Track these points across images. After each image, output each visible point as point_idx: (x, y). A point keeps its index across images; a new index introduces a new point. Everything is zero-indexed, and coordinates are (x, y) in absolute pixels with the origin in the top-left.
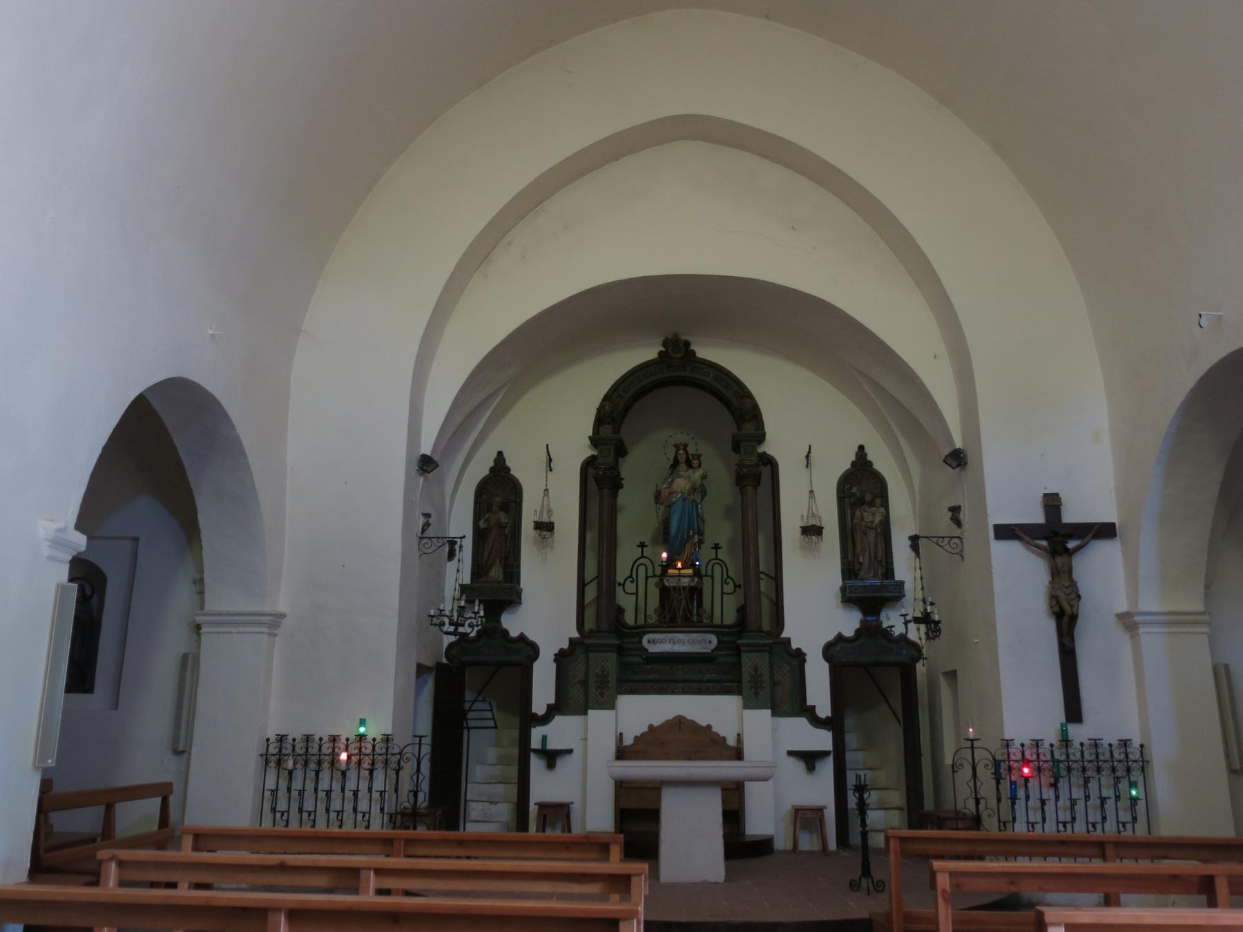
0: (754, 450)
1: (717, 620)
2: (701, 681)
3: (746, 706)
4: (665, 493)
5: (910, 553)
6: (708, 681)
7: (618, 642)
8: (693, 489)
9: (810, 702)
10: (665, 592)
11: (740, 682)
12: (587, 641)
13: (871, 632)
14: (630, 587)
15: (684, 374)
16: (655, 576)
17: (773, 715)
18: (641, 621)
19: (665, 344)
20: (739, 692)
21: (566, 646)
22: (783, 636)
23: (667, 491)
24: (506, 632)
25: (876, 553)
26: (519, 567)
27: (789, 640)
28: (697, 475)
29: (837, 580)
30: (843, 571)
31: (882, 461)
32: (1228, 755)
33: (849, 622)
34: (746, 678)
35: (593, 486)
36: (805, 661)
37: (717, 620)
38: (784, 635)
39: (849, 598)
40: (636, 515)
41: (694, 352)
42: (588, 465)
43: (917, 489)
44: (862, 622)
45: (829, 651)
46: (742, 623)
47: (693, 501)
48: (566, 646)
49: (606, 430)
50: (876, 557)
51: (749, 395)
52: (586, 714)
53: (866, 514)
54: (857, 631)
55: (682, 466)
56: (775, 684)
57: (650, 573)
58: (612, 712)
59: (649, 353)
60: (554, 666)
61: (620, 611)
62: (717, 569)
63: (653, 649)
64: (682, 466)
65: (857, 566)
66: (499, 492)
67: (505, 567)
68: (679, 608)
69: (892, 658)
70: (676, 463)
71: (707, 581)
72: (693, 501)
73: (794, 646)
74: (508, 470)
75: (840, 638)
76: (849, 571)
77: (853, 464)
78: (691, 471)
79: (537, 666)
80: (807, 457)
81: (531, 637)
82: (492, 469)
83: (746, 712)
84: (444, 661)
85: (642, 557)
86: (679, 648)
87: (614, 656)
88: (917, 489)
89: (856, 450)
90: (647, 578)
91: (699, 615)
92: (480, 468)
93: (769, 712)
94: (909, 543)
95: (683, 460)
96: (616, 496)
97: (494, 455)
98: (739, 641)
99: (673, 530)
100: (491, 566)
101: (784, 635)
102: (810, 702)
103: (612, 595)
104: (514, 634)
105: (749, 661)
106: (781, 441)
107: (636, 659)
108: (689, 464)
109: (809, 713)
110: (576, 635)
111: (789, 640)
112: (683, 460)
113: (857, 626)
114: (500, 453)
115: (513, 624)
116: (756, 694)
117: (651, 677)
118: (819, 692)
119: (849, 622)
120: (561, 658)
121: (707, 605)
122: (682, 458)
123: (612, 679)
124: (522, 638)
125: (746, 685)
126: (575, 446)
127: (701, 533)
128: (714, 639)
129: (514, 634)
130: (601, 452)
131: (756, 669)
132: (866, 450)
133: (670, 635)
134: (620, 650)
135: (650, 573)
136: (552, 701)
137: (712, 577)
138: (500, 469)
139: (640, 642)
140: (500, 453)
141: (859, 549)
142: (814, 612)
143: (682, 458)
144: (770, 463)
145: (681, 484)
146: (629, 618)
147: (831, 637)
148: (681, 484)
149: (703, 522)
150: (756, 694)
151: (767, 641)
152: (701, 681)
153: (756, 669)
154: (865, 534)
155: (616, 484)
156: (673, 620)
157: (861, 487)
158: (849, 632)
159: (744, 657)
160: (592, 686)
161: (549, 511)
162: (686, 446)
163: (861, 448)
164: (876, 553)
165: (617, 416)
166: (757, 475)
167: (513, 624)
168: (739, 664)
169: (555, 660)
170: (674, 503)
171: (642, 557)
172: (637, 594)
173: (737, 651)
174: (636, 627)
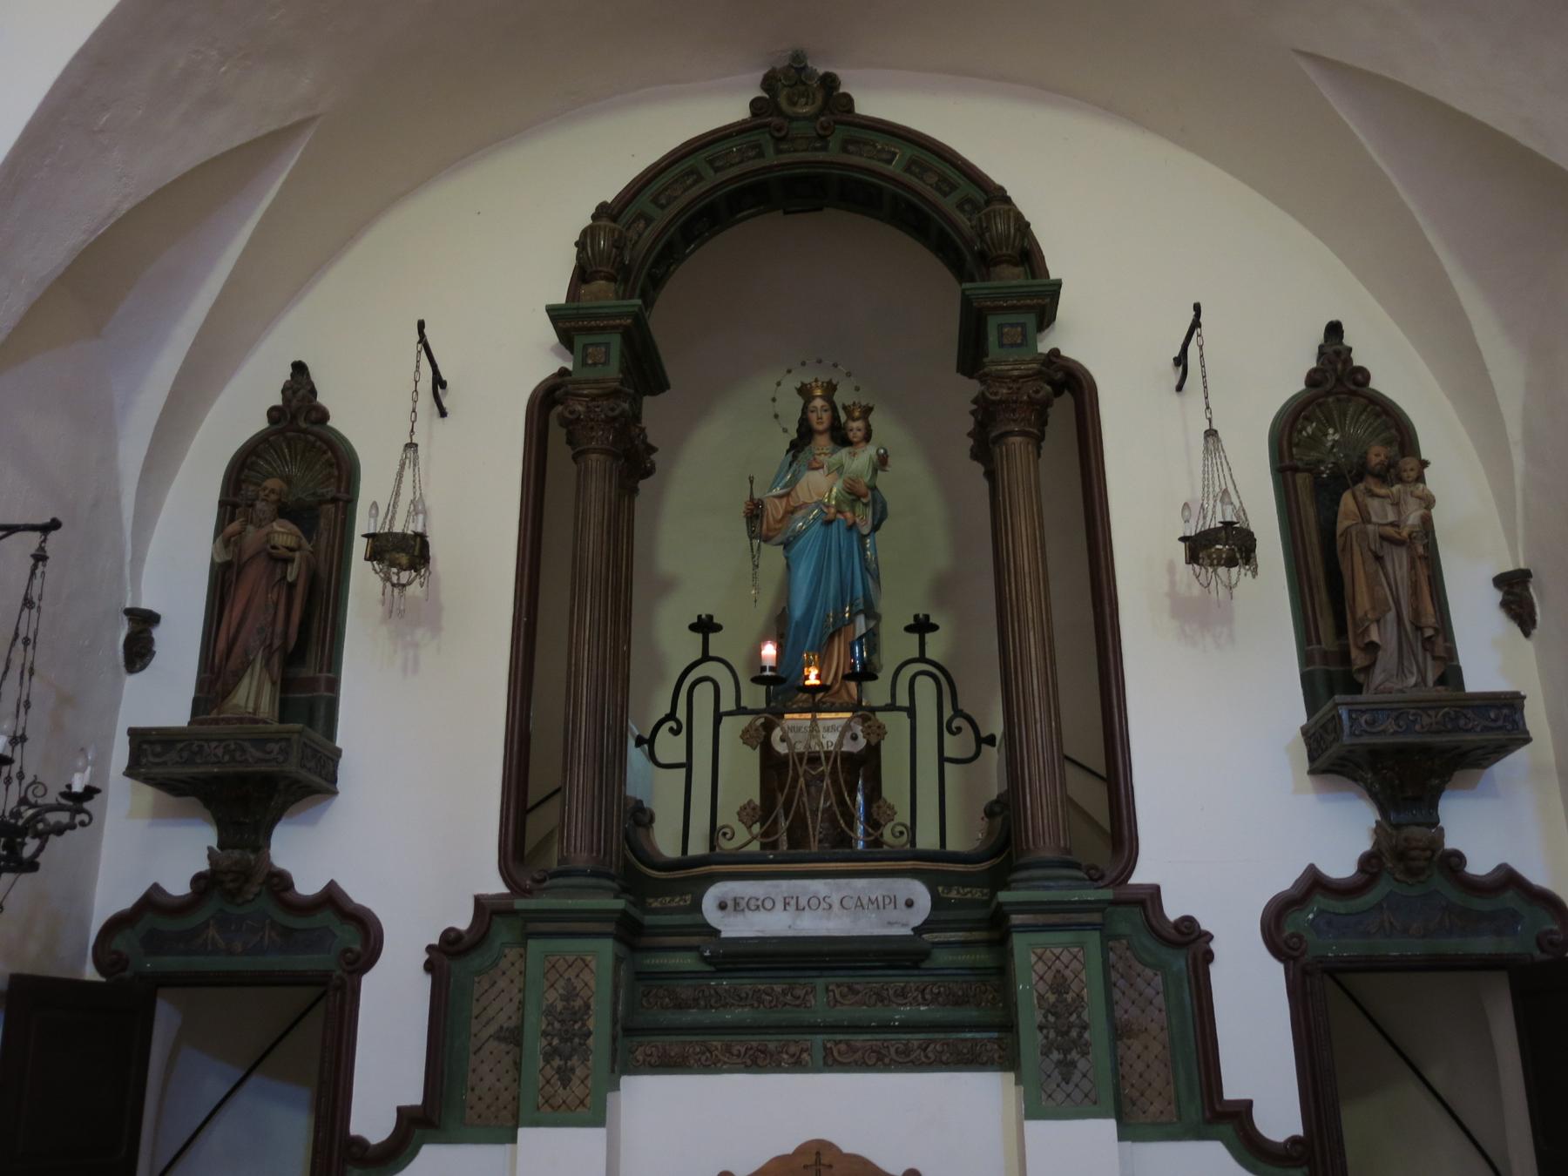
0: (1026, 341)
1: (927, 839)
2: (885, 1027)
3: (1033, 1111)
4: (774, 510)
5: (1500, 624)
6: (908, 1027)
7: (619, 904)
8: (853, 495)
9: (1232, 1091)
10: (773, 767)
11: (1008, 1027)
12: (520, 904)
13: (1409, 857)
14: (670, 747)
15: (821, 156)
16: (740, 710)
17: (1122, 1136)
18: (698, 847)
19: (769, 83)
20: (1006, 1059)
21: (463, 920)
22: (1137, 878)
23: (781, 506)
24: (281, 882)
25: (1417, 613)
26: (334, 685)
27: (1155, 891)
28: (859, 461)
29: (1289, 710)
30: (1307, 681)
31: (1395, 369)
32: (615, 1004)
33: (1337, 834)
34: (1029, 1017)
35: (557, 435)
36: (1209, 956)
37: (927, 839)
38: (1141, 876)
39: (1331, 756)
40: (701, 562)
41: (848, 100)
42: (546, 403)
43: (1514, 430)
44: (1379, 830)
45: (1282, 925)
46: (1006, 841)
47: (852, 527)
48: (463, 921)
49: (602, 293)
50: (1418, 628)
51: (999, 196)
52: (513, 1139)
53: (1374, 505)
54: (1366, 862)
55: (822, 442)
56: (1119, 1032)
57: (727, 704)
58: (599, 1134)
59: (731, 109)
60: (427, 980)
61: (641, 817)
62: (925, 687)
63: (734, 927)
64: (822, 442)
65: (1358, 658)
66: (295, 479)
67: (286, 684)
68: (817, 812)
69: (1484, 945)
70: (805, 434)
71: (895, 723)
72: (852, 527)
73: (1173, 910)
74: (324, 416)
75: (1314, 883)
76: (1330, 672)
77: (1313, 379)
78: (843, 453)
79: (370, 984)
80: (1181, 360)
81: (359, 895)
82: (274, 414)
83: (1037, 1130)
84: (90, 973)
85: (706, 657)
86: (812, 925)
87: (606, 949)
88: (1514, 430)
89: (1319, 337)
90: (718, 717)
91: (873, 824)
92: (241, 411)
93: (1110, 1125)
94: (1497, 596)
95: (822, 429)
96: (633, 491)
97: (286, 374)
98: (1003, 896)
99: (798, 611)
100: (238, 677)
101: (1141, 876)
102: (1232, 1091)
103: (612, 766)
104: (307, 885)
105: (1034, 958)
106: (1103, 322)
107: (686, 961)
108: (841, 438)
109: (1233, 1123)
110: (495, 886)
111: (1155, 891)
112: (822, 429)
113: (1366, 845)
114: (299, 368)
115: (306, 854)
116: (1067, 1067)
117: (728, 1016)
118: (1258, 1053)
119: (1337, 834)
120: (447, 956)
121: (894, 787)
122: (820, 420)
123: (599, 1024)
124: (332, 898)
125: (1030, 1040)
126: (511, 350)
127: (871, 612)
128: (920, 893)
129: (307, 885)
130: (583, 363)
131: (1059, 985)
132: (1348, 340)
133: (785, 886)
134: (629, 932)
135: (727, 704)
136: (414, 1097)
137: (911, 711)
138: (299, 422)
139: (697, 906)
140: (299, 368)
141: (1363, 603)
142: (1226, 798)
143: (820, 420)
144: (1073, 384)
145: (816, 488)
146: (666, 841)
147: (1284, 880)
148: (816, 488)
149: (877, 579)
150: (1067, 1067)
151: (1091, 895)
152: (885, 1027)
153: (1059, 985)
154: (1379, 559)
155: (634, 462)
156: (798, 837)
157: (1339, 442)
158: (1341, 866)
159: (1019, 942)
160: (535, 1045)
161: (418, 507)
162: (830, 389)
163: (1334, 330)
164: (1417, 613)
165: (638, 261)
166: (1037, 416)
167: (306, 854)
168: (1002, 973)
169: (429, 967)
170: (798, 535)
171: (706, 657)
172: (688, 766)
173: (997, 929)
174: (686, 863)
